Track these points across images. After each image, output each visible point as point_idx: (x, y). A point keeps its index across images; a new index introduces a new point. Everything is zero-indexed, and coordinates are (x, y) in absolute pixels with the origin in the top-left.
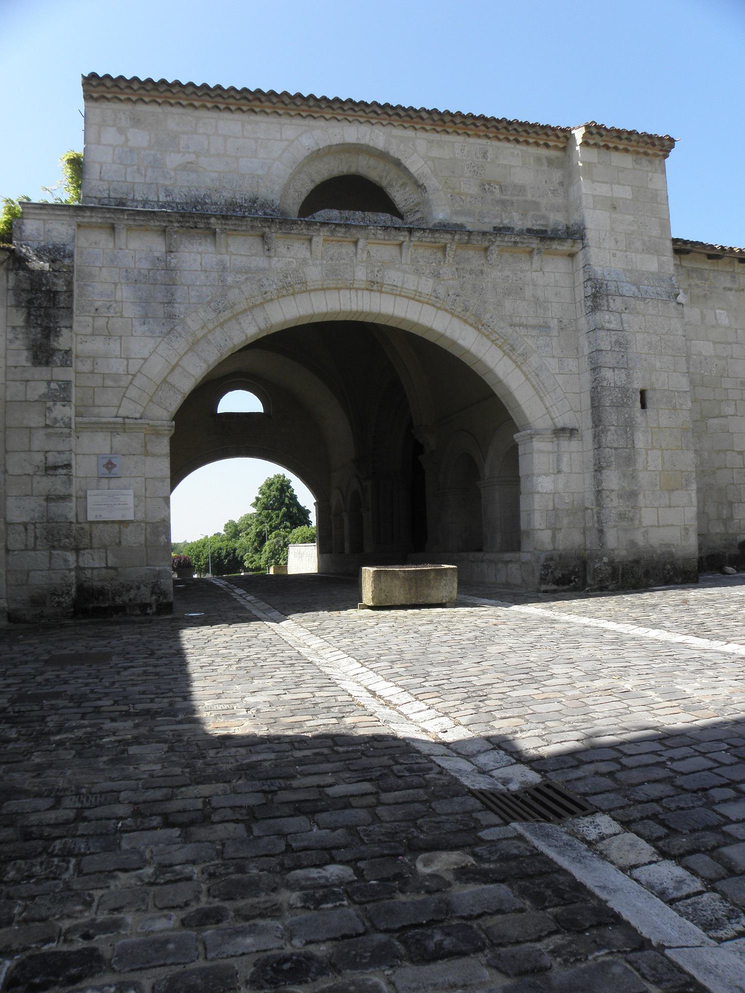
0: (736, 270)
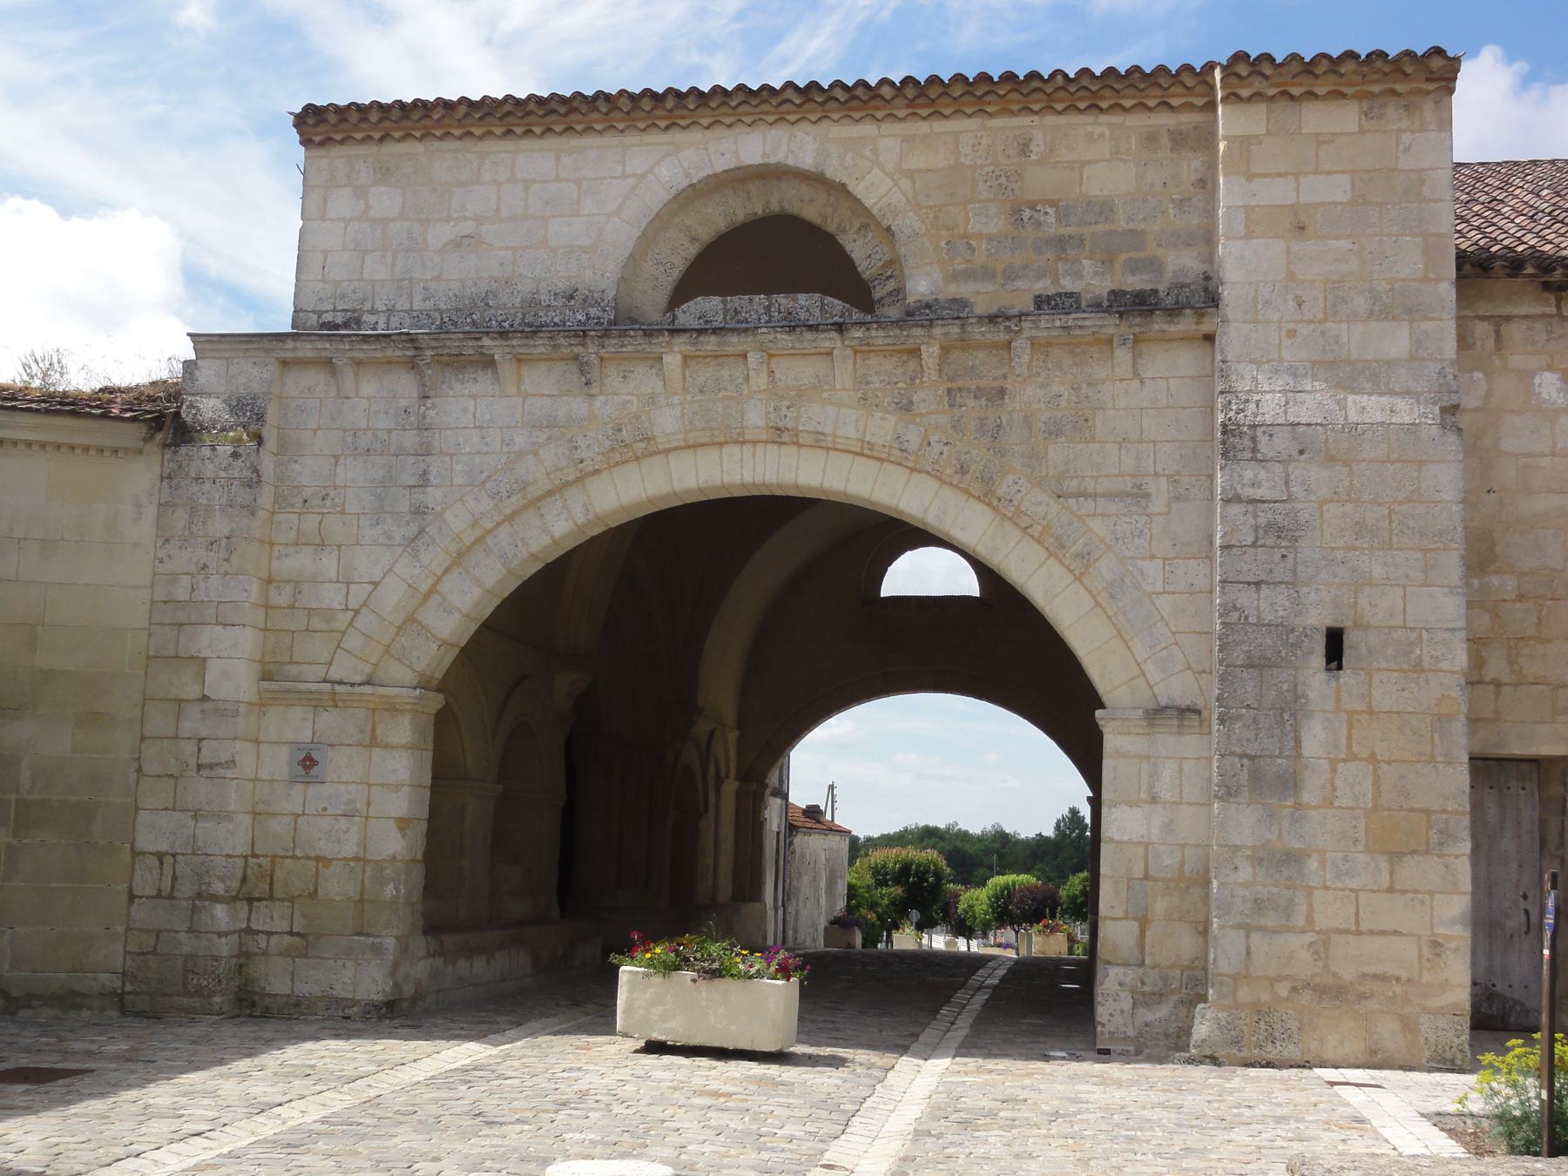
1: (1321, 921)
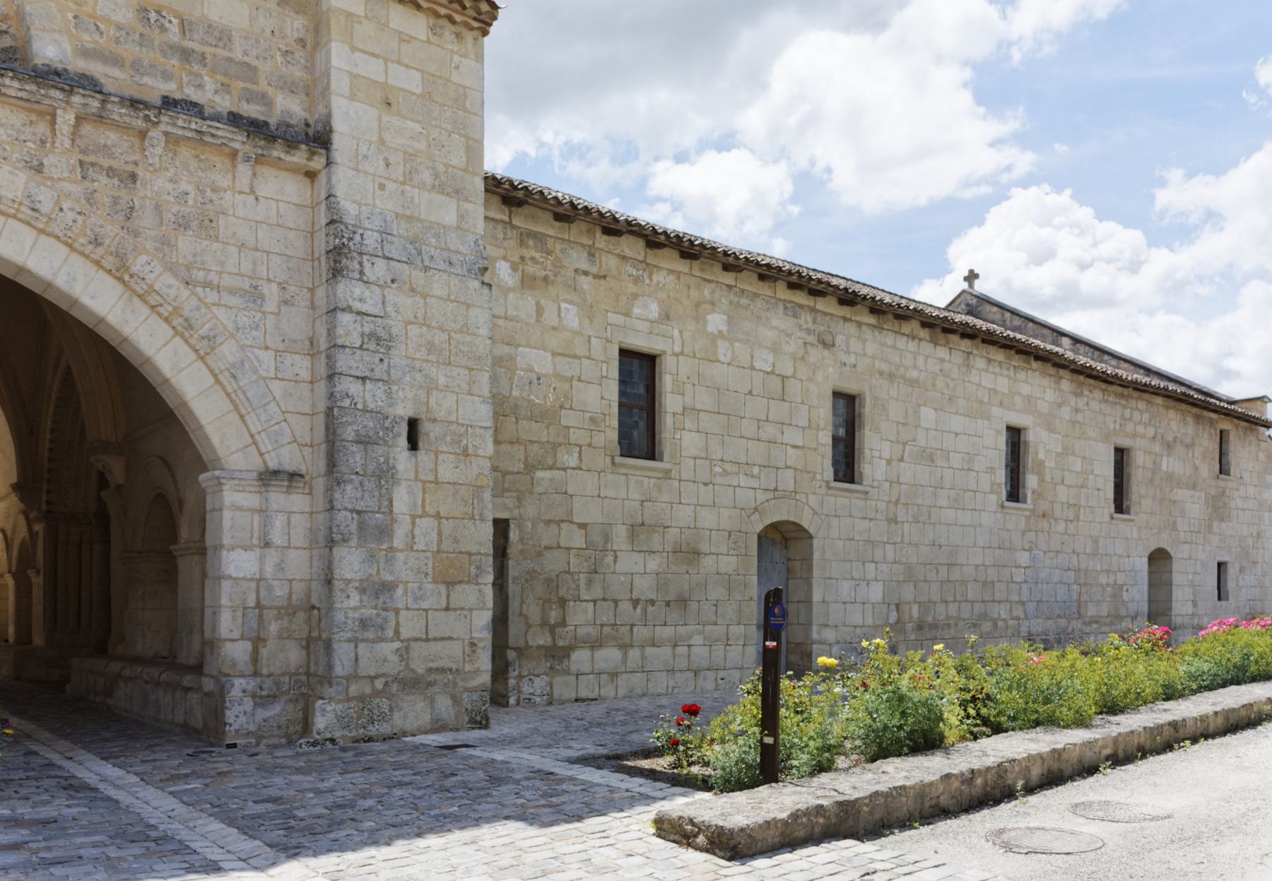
0: (597, 245)
1: (405, 633)
